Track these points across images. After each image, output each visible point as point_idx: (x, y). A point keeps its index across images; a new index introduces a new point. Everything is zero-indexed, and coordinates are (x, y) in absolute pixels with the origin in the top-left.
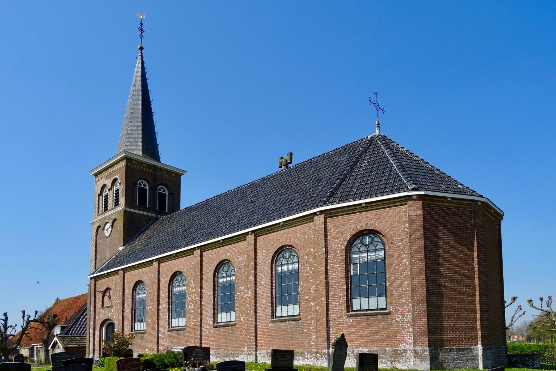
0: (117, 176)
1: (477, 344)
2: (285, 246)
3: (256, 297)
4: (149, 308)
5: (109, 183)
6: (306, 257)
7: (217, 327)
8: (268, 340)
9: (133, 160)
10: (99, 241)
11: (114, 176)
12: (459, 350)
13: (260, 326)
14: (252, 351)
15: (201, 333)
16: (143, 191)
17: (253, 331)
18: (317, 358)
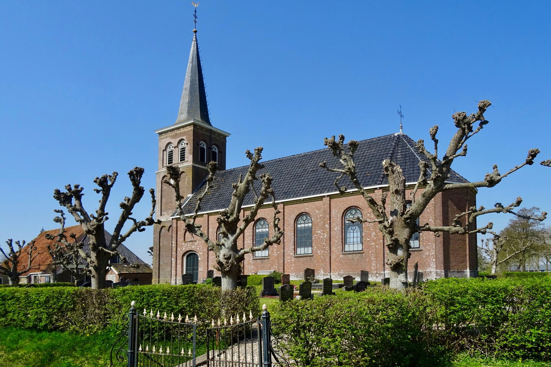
0: (184, 138)
1: (467, 269)
2: (353, 206)
3: (330, 238)
5: (175, 142)
6: (368, 215)
7: (297, 257)
8: (340, 266)
9: (197, 126)
11: (180, 137)
12: (458, 272)
13: (333, 256)
14: (327, 273)
15: (284, 261)
16: (202, 149)
17: (328, 260)
18: (376, 276)
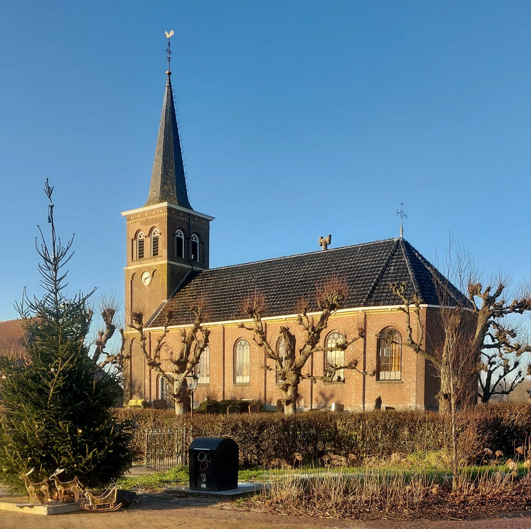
4: (213, 365)
10: (135, 289)
15: (265, 389)
